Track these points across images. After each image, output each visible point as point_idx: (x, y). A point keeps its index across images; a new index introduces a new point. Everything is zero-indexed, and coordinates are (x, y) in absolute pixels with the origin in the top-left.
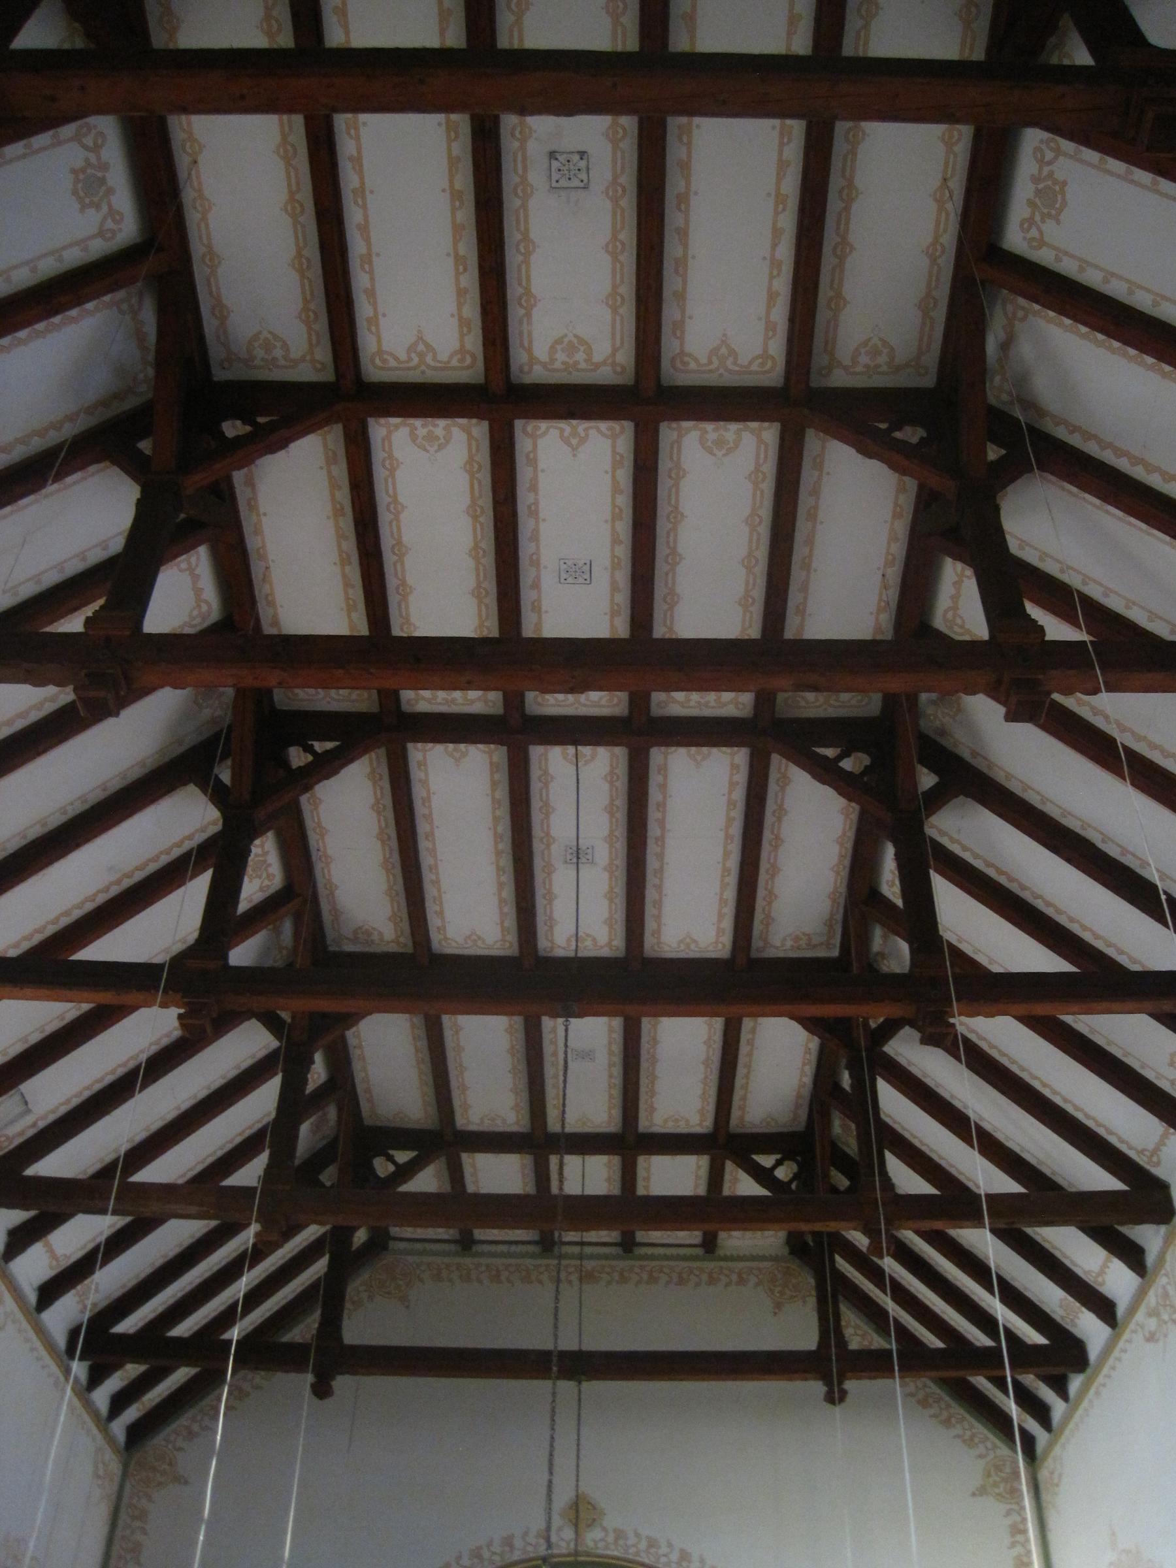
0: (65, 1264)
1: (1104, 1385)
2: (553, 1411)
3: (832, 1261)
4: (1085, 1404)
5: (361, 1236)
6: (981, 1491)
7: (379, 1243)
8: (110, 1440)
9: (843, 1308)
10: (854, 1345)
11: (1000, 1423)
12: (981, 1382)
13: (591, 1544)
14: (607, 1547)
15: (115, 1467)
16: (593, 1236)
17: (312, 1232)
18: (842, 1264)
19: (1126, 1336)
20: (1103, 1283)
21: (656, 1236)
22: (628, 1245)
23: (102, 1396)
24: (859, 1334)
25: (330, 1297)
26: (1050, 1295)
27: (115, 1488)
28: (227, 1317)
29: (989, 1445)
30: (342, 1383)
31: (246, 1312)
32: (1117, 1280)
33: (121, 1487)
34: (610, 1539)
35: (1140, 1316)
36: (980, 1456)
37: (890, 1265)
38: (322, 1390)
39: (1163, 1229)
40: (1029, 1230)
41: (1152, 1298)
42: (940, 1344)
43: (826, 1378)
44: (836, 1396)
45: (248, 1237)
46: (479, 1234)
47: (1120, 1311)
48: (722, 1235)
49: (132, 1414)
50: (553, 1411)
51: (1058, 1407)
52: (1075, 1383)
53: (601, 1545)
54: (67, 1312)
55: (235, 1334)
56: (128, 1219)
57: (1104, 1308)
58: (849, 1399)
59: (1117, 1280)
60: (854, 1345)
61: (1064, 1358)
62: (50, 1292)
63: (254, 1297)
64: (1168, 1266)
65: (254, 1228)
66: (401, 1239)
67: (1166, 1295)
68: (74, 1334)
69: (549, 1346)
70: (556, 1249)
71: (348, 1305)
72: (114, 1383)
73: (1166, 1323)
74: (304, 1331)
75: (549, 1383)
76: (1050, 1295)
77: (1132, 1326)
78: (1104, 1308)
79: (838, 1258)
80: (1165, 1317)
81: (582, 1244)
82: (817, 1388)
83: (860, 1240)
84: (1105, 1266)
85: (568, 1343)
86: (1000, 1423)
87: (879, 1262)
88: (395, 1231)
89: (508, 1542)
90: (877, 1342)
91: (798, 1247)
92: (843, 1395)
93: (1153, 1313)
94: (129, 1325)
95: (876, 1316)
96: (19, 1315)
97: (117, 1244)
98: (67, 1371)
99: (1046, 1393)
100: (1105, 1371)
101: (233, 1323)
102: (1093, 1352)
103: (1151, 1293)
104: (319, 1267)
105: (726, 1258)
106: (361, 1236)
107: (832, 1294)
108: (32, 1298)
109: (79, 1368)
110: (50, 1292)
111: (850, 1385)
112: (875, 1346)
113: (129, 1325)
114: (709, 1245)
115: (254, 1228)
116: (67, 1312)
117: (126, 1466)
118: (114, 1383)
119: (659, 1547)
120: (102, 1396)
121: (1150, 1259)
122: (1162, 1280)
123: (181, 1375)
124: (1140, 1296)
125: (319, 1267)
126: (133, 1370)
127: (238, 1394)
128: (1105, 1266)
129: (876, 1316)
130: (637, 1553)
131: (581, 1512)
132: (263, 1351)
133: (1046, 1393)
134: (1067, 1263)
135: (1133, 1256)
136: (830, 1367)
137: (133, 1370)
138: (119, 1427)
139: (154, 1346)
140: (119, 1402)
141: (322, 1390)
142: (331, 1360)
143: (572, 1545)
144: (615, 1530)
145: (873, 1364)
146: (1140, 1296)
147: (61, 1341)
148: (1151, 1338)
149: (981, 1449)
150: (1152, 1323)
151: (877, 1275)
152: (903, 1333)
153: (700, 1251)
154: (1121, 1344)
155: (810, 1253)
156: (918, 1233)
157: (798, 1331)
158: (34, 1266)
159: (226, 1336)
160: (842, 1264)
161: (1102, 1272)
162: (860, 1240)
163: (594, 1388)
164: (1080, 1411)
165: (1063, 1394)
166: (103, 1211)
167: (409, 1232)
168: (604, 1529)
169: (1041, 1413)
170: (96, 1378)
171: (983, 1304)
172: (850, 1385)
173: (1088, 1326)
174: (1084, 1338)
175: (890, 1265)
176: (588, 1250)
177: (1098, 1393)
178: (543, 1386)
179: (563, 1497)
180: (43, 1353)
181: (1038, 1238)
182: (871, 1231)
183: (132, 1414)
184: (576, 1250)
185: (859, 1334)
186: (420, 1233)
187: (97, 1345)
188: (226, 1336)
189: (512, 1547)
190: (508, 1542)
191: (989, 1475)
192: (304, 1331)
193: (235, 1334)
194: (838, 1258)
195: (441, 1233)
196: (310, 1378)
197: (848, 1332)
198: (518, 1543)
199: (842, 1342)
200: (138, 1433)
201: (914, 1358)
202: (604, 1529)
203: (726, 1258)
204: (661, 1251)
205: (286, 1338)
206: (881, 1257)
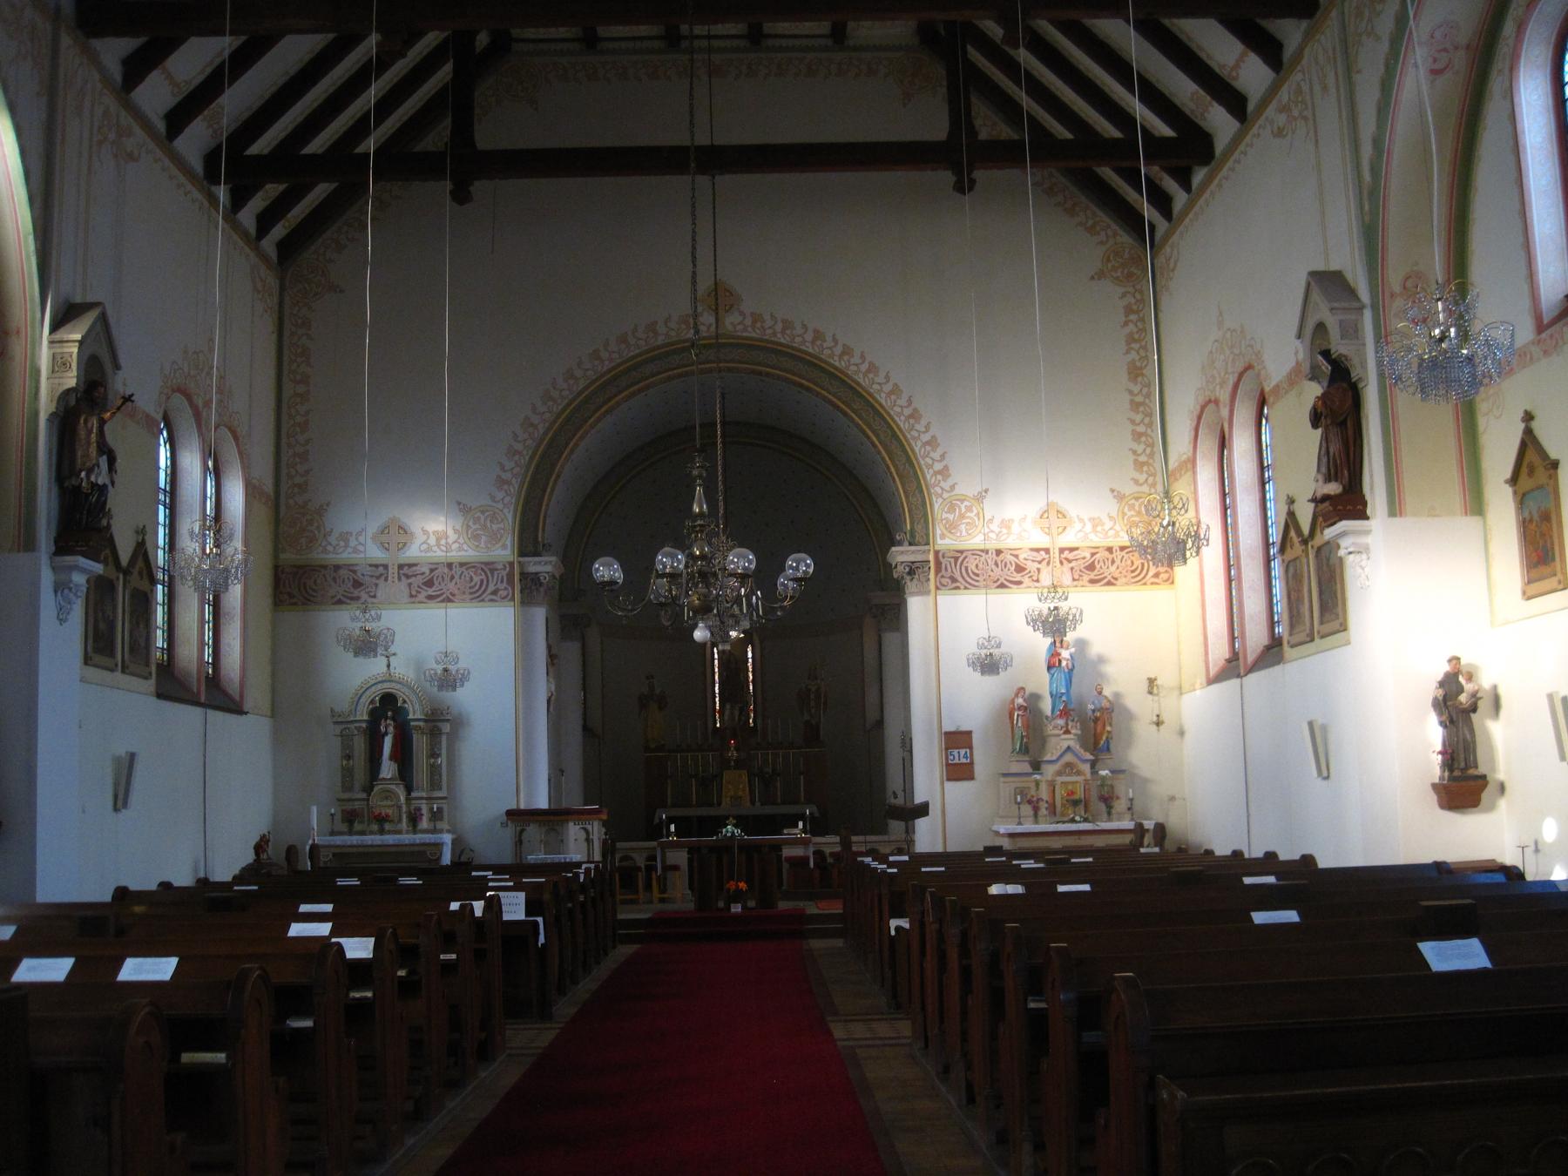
0: (186, 90)
1: (1226, 178)
2: (693, 206)
3: (965, 52)
4: (1207, 195)
5: (483, 39)
6: (1100, 275)
7: (501, 45)
8: (263, 257)
9: (974, 99)
10: (983, 135)
11: (1132, 221)
12: (1107, 173)
13: (730, 328)
14: (745, 330)
15: (272, 281)
16: (719, 29)
17: (431, 39)
18: (974, 55)
19: (1254, 130)
20: (1236, 78)
21: (783, 27)
22: (755, 37)
23: (248, 216)
24: (989, 125)
25: (458, 104)
26: (1182, 88)
27: (276, 300)
28: (360, 129)
29: (1110, 232)
30: (479, 187)
31: (367, 115)
32: (1252, 74)
33: (281, 304)
34: (748, 322)
35: (1270, 111)
36: (1102, 243)
37: (1024, 56)
38: (461, 195)
39: (1304, 24)
40: (1166, 22)
41: (1284, 94)
42: (1070, 136)
43: (957, 169)
44: (963, 186)
45: (371, 44)
46: (602, 31)
47: (1251, 107)
48: (851, 25)
49: (279, 231)
50: (693, 206)
51: (1180, 198)
52: (1199, 176)
53: (740, 327)
54: (195, 140)
55: (370, 145)
56: (244, 38)
57: (1236, 103)
58: (978, 186)
59: (1252, 74)
60: (983, 135)
61: (1190, 151)
62: (178, 119)
63: (385, 107)
64: (1304, 62)
65: (374, 39)
66: (523, 40)
67: (1299, 91)
68: (211, 159)
69: (688, 143)
70: (685, 44)
71: (477, 111)
72: (257, 204)
73: (1295, 119)
74: (436, 139)
75: (687, 178)
76: (1182, 88)
77: (1261, 122)
78: (1236, 103)
79: (969, 48)
80: (1296, 113)
81: (709, 37)
82: (948, 177)
83: (994, 30)
84: (1241, 59)
85: (702, 140)
86: (1132, 221)
87: (1012, 52)
88: (516, 32)
89: (652, 328)
90: (1006, 132)
91: (928, 36)
92: (972, 182)
93: (1284, 109)
94: (261, 146)
95: (1010, 109)
96: (152, 145)
97: (241, 61)
98: (213, 200)
99: (1170, 185)
100: (1230, 164)
101: (368, 134)
102: (1220, 146)
103: (1285, 88)
104: (445, 73)
105: (856, 49)
106: (483, 39)
107: (964, 86)
108: (161, 126)
109: (222, 192)
110: (178, 119)
111: (978, 174)
112: (1003, 136)
113: (261, 146)
114: (838, 35)
115: (374, 39)
116: (195, 140)
117: (282, 280)
118: (257, 204)
119: (876, 375)
120: (248, 216)
121: (1288, 53)
122: (1297, 77)
123: (321, 191)
124: (1273, 90)
125: (445, 73)
126: (272, 190)
127: (380, 205)
128: (1241, 59)
129: (1010, 109)
130: (775, 334)
131: (721, 298)
132: (400, 161)
133: (1170, 185)
134: (1203, 56)
135: (1271, 51)
136: (960, 159)
137: (272, 190)
138: (269, 244)
139: (289, 164)
140: (266, 221)
141: (461, 195)
142: (467, 167)
143: (713, 328)
144: (752, 314)
145: (1004, 154)
146: (1273, 90)
147: (198, 166)
148: (1279, 133)
149: (1103, 236)
150: (1282, 119)
151: (1012, 68)
152: (1035, 124)
153: (830, 42)
154: (1248, 139)
155: (944, 43)
156: (1052, 22)
157: (932, 124)
158: (156, 94)
159: (360, 149)
160: (974, 55)
161: (1237, 66)
162: (994, 30)
163: (726, 181)
164: (1201, 202)
165: (1186, 185)
166: (219, 32)
167: (530, 33)
168: (742, 313)
169: (1162, 202)
170: (238, 201)
171: (1123, 104)
172: (978, 174)
173: (1218, 120)
174: (1211, 131)
175: (1024, 56)
176: (716, 43)
177: (1220, 185)
178: (680, 182)
179: (705, 284)
180: (182, 179)
181: (1174, 29)
182: (1007, 20)
183: (279, 231)
184: (704, 43)
185: (989, 125)
186: (542, 33)
187: (233, 169)
188: (360, 149)
189: (656, 333)
190: (652, 328)
191: (1108, 260)
192: (436, 139)
193: (370, 145)
194: (969, 48)
195: (563, 32)
196: (448, 185)
197: (978, 123)
198: (661, 329)
199: (972, 132)
200: (288, 249)
201: (1045, 149)
202: (742, 313)
203: (856, 49)
204: (791, 42)
205: (419, 147)
206: (1017, 47)
